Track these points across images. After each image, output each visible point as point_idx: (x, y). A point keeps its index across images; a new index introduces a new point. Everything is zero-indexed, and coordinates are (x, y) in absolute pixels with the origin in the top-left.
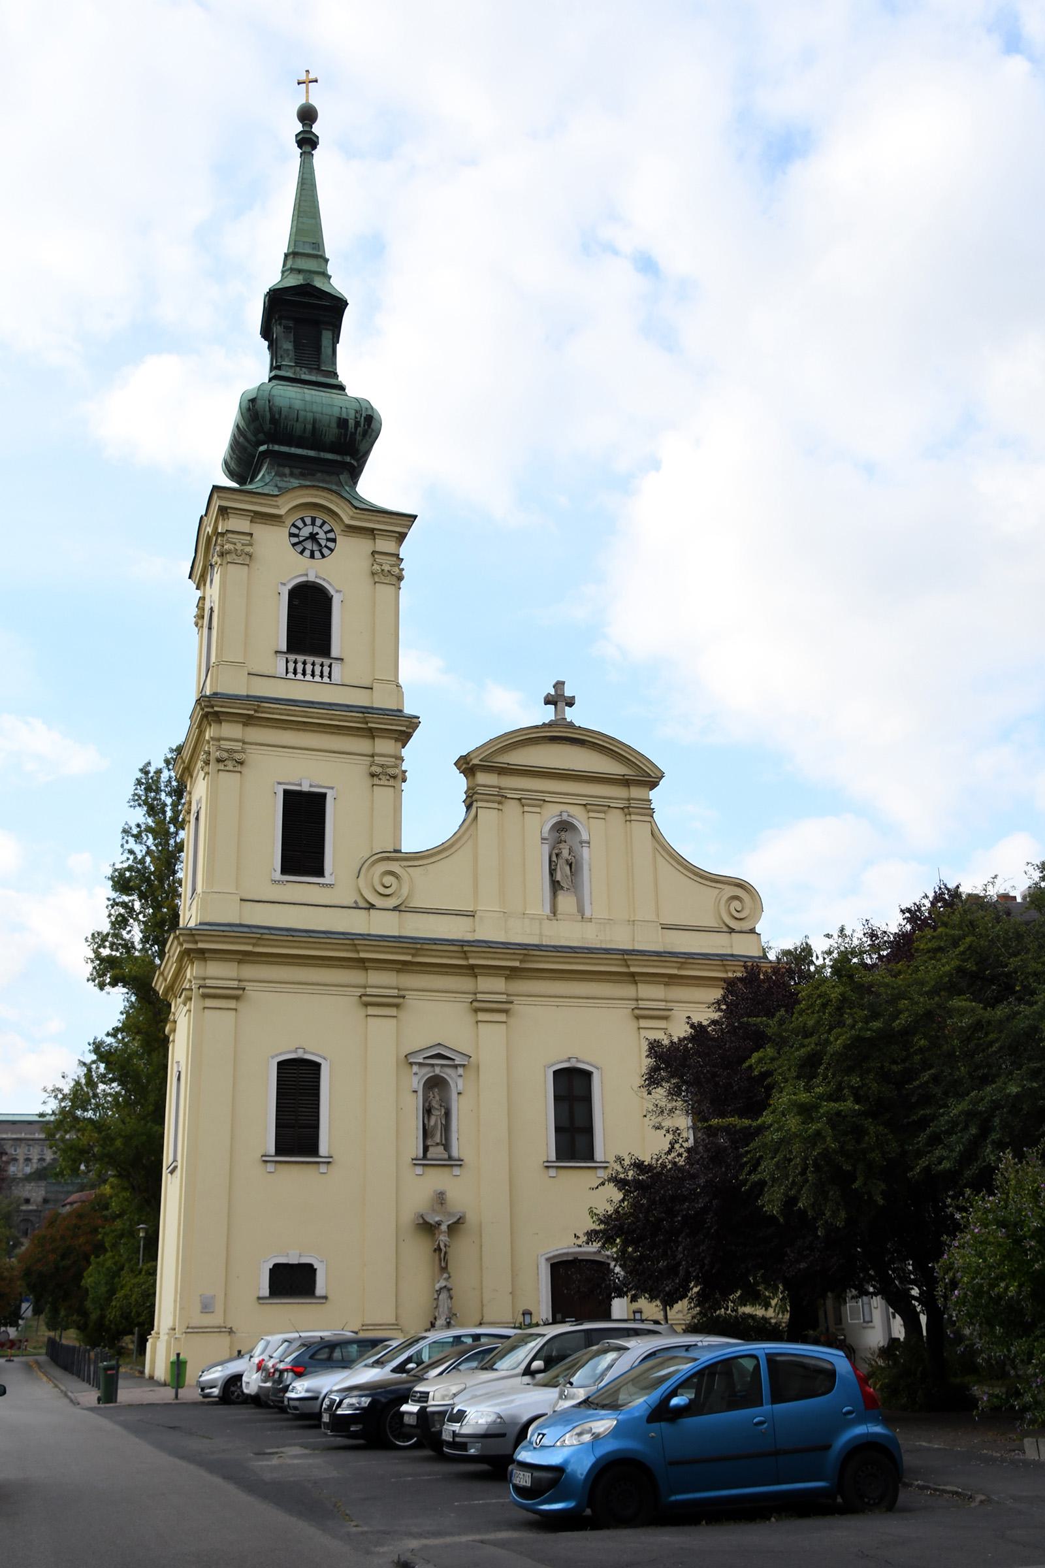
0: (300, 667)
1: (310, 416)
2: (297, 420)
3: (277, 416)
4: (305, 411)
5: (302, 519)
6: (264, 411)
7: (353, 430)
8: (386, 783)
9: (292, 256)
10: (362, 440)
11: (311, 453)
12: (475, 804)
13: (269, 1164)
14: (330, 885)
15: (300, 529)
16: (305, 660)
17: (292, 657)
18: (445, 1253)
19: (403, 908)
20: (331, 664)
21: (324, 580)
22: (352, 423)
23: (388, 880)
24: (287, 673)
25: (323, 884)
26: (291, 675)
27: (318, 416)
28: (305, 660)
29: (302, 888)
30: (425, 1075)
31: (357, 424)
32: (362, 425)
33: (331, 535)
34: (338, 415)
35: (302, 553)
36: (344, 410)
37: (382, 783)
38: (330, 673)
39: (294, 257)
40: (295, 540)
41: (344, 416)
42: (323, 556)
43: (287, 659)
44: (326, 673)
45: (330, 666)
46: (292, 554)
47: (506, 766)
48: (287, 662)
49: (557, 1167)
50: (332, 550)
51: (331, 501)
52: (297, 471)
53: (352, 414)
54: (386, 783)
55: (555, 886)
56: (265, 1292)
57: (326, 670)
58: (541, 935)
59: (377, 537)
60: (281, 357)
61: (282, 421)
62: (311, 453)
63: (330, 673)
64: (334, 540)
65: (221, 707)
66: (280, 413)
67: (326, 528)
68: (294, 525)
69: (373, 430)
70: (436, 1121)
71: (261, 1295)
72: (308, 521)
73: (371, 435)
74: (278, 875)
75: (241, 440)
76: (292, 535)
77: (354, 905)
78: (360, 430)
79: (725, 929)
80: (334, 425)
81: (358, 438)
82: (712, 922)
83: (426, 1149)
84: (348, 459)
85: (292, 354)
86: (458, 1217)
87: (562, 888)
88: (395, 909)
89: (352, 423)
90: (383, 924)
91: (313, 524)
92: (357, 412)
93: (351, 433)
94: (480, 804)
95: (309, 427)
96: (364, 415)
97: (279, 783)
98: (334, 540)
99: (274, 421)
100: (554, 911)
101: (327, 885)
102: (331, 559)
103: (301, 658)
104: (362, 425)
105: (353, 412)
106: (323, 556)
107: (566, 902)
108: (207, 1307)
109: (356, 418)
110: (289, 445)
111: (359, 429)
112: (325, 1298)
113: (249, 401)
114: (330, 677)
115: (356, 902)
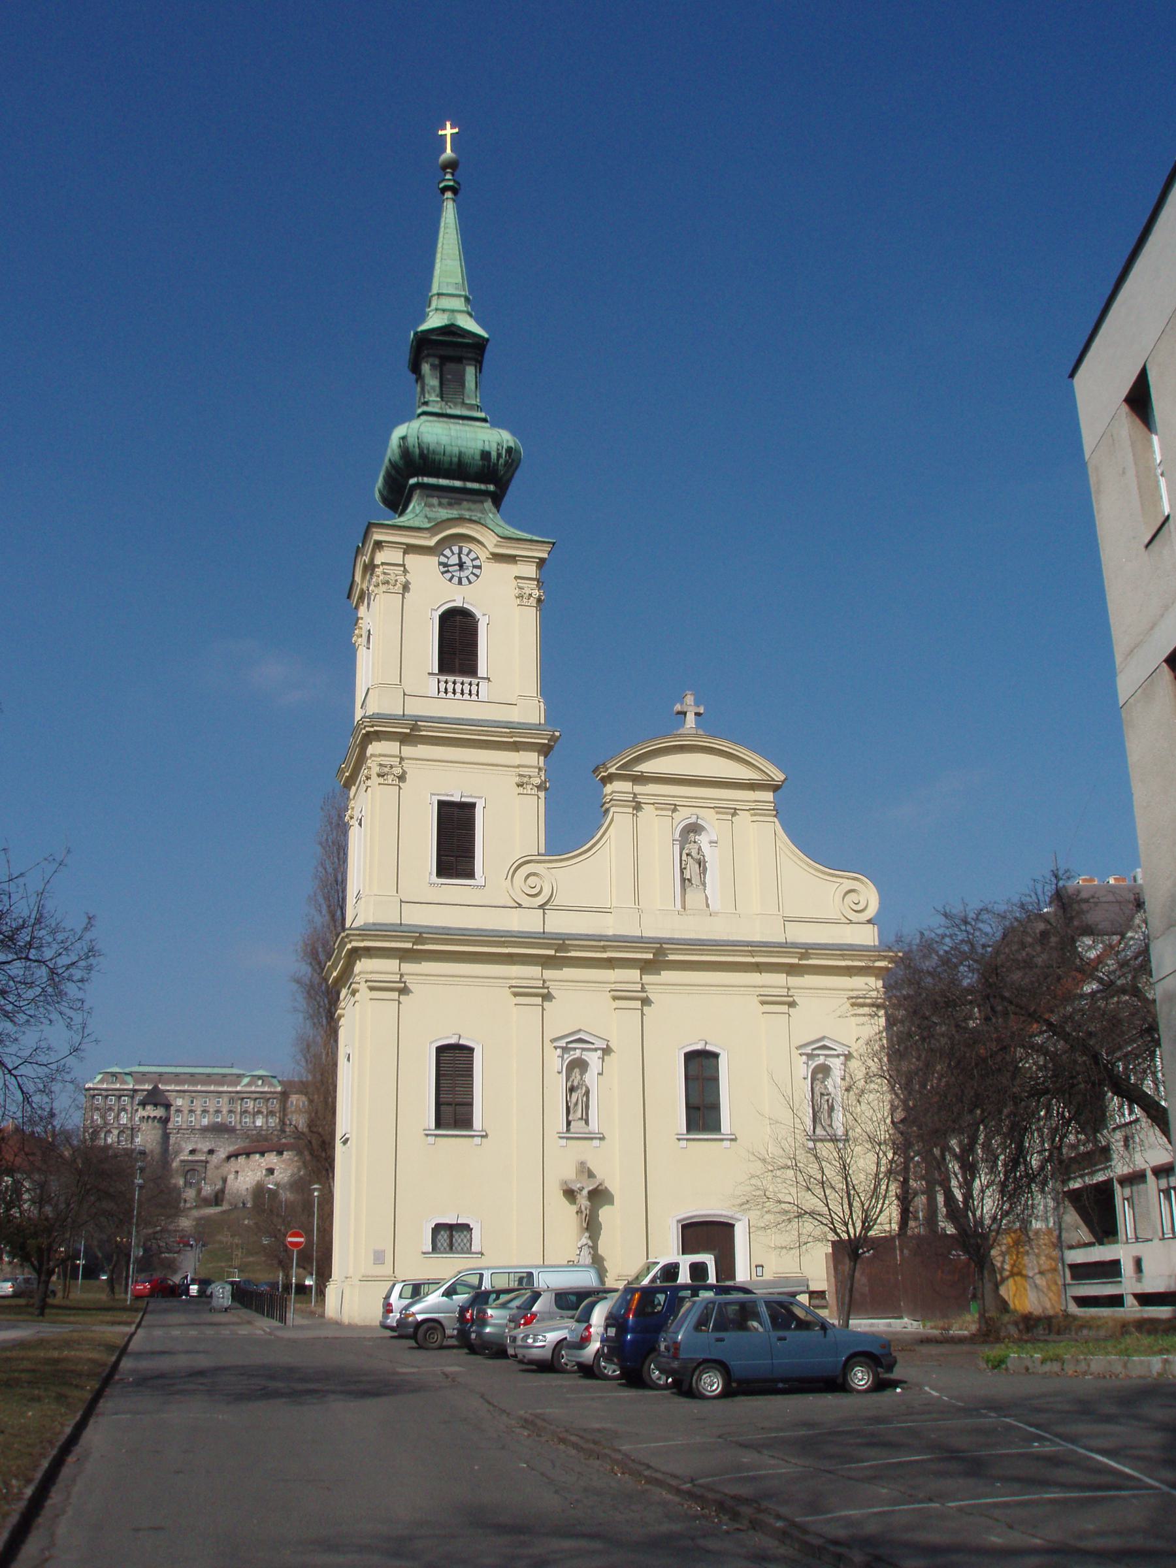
0: (450, 687)
2: (444, 455)
3: (425, 452)
4: (451, 445)
6: (414, 447)
9: (436, 297)
11: (458, 484)
12: (613, 809)
13: (429, 1138)
15: (448, 558)
17: (443, 678)
20: (479, 682)
21: (471, 604)
22: (494, 454)
23: (532, 881)
25: (474, 886)
26: (442, 694)
27: (463, 450)
29: (455, 888)
31: (499, 456)
32: (504, 456)
33: (477, 563)
34: (482, 448)
36: (487, 443)
38: (478, 692)
39: (438, 298)
41: (487, 448)
42: (470, 582)
44: (474, 691)
45: (478, 685)
46: (442, 580)
48: (439, 682)
50: (478, 576)
51: (477, 531)
52: (445, 501)
53: (494, 446)
60: (429, 392)
61: (430, 456)
62: (458, 484)
63: (478, 692)
64: (479, 567)
66: (428, 449)
67: (472, 556)
71: (424, 1251)
75: (393, 472)
80: (478, 457)
82: (834, 915)
83: (569, 1123)
86: (598, 1184)
89: (494, 454)
93: (494, 464)
96: (505, 446)
97: (432, 794)
98: (479, 567)
99: (423, 455)
102: (478, 584)
103: (451, 679)
104: (504, 456)
106: (470, 582)
107: (694, 897)
108: (379, 1258)
109: (498, 450)
113: (400, 438)
114: (477, 695)
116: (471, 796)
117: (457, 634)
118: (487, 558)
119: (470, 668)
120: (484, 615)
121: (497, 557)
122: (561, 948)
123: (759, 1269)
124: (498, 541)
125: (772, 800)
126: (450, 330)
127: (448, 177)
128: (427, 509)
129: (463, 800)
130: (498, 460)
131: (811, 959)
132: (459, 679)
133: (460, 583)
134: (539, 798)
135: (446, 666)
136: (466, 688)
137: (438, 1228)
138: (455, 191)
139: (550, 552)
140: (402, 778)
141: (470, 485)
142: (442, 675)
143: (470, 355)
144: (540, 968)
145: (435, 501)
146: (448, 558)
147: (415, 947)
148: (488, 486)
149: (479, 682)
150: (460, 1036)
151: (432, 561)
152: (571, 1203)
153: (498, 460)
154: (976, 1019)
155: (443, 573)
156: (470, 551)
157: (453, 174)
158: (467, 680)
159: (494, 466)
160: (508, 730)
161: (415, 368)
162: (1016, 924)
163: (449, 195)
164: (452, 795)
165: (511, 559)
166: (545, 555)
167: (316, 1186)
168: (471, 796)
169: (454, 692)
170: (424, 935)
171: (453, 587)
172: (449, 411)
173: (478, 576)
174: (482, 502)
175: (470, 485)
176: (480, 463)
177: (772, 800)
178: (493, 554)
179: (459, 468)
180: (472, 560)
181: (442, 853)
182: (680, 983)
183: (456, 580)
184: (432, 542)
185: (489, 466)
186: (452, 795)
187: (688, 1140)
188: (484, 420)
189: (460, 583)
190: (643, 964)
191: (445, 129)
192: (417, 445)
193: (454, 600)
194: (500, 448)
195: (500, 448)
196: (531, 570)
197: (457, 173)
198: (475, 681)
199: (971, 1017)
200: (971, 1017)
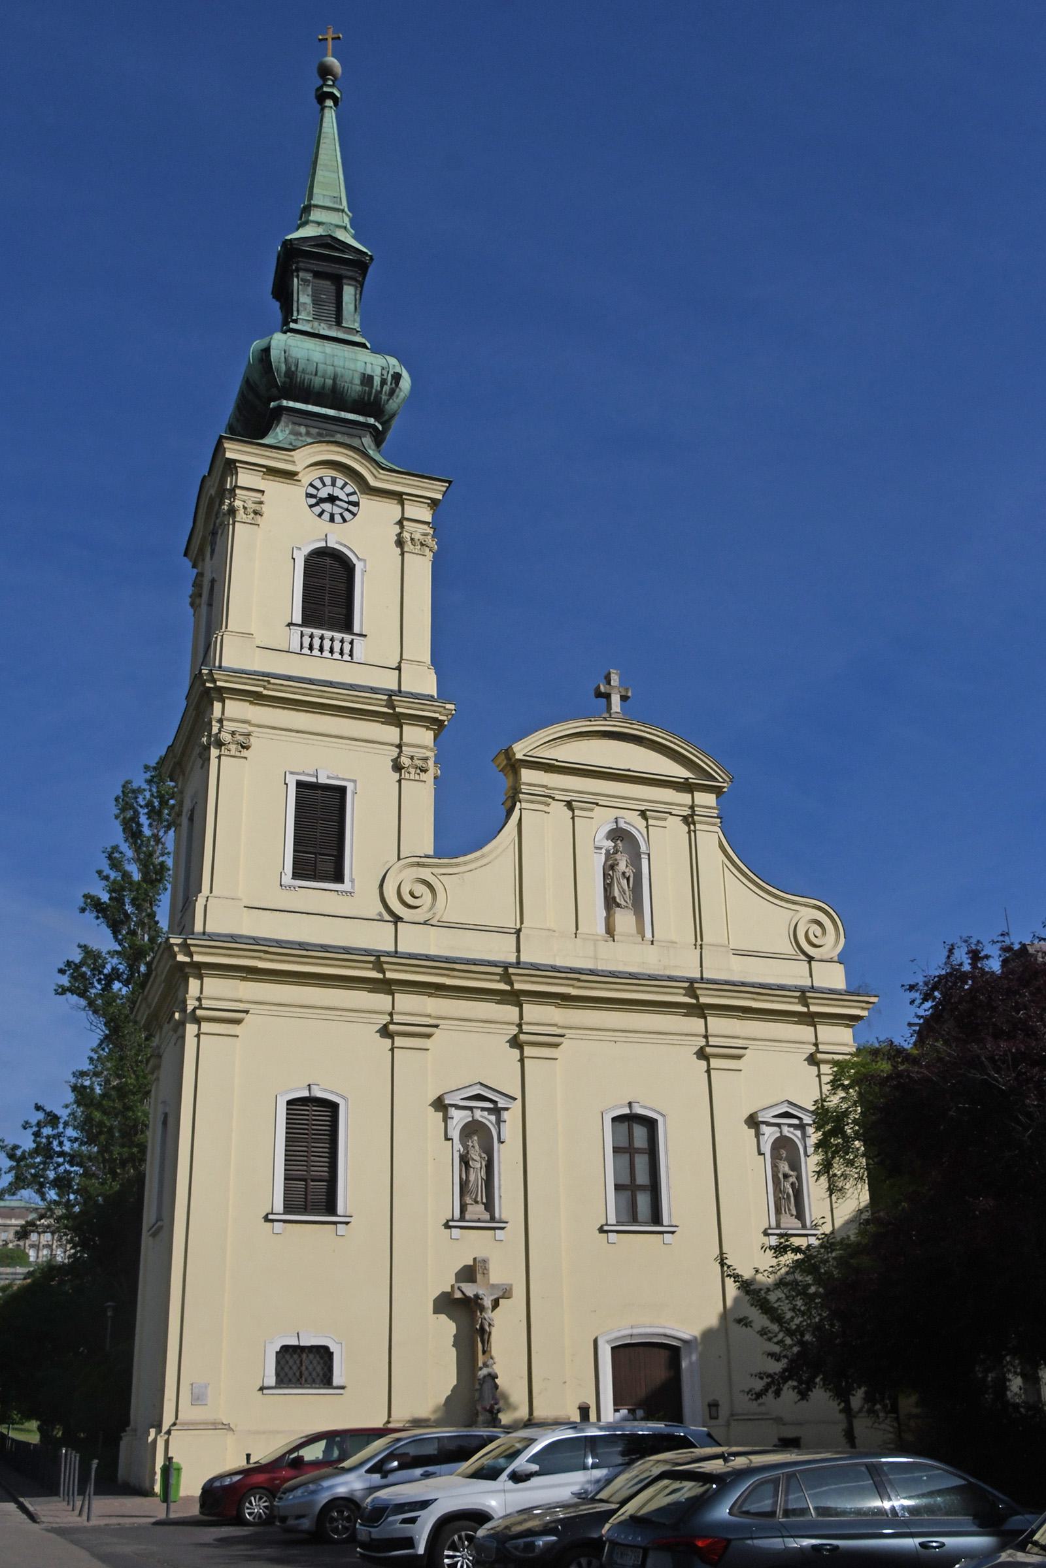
1: (330, 370)
2: (316, 375)
3: (293, 369)
5: (321, 479)
7: (379, 389)
8: (417, 777)
10: (388, 400)
11: (331, 412)
14: (351, 893)
15: (318, 490)
16: (323, 635)
17: (308, 631)
18: (490, 1333)
19: (434, 922)
20: (353, 640)
22: (377, 381)
23: (420, 889)
24: (302, 648)
25: (342, 892)
26: (306, 651)
27: (339, 370)
28: (323, 635)
30: (461, 1119)
31: (383, 382)
32: (389, 383)
34: (362, 371)
35: (320, 515)
36: (369, 366)
37: (412, 777)
38: (351, 650)
40: (313, 501)
41: (369, 372)
43: (302, 632)
45: (352, 643)
46: (309, 516)
49: (285, 1221)
50: (354, 515)
52: (314, 431)
54: (417, 777)
55: (610, 903)
56: (271, 1380)
57: (347, 647)
58: (596, 958)
59: (406, 502)
61: (299, 374)
62: (331, 412)
63: (351, 650)
64: (356, 504)
65: (226, 681)
66: (297, 366)
68: (311, 485)
69: (400, 389)
70: (476, 1176)
72: (328, 481)
73: (398, 396)
74: (288, 878)
76: (309, 495)
77: (378, 918)
78: (386, 388)
80: (357, 381)
81: (384, 397)
84: (372, 421)
85: (310, 308)
87: (619, 905)
88: (425, 923)
89: (377, 381)
90: (414, 940)
91: (333, 484)
92: (383, 368)
94: (524, 805)
95: (329, 382)
96: (391, 372)
98: (356, 504)
99: (290, 374)
100: (610, 931)
101: (346, 892)
102: (353, 524)
103: (318, 632)
104: (389, 383)
105: (380, 368)
106: (345, 521)
109: (382, 375)
110: (307, 402)
111: (385, 387)
112: (343, 1388)
114: (351, 655)
115: (380, 914)
117: (327, 592)
119: (345, 623)
123: (714, 1409)
125: (715, 805)
126: (329, 242)
128: (292, 437)
130: (382, 387)
132: (328, 634)
133: (332, 519)
137: (286, 1352)
139: (445, 492)
141: (344, 415)
142: (307, 627)
143: (350, 274)
145: (303, 430)
146: (318, 490)
148: (368, 418)
149: (353, 640)
152: (457, 1274)
153: (382, 387)
155: (311, 506)
158: (338, 636)
159: (376, 396)
161: (283, 294)
163: (329, 103)
166: (440, 497)
167: (109, 1304)
169: (321, 650)
171: (324, 525)
172: (322, 332)
173: (354, 515)
175: (344, 415)
176: (359, 388)
177: (715, 805)
179: (333, 395)
181: (301, 848)
182: (598, 1026)
183: (326, 516)
185: (370, 394)
187: (285, 1221)
188: (363, 346)
189: (332, 519)
191: (327, 33)
192: (283, 359)
194: (385, 373)
195: (385, 373)
198: (348, 637)
199: (169, 815)
200: (169, 815)
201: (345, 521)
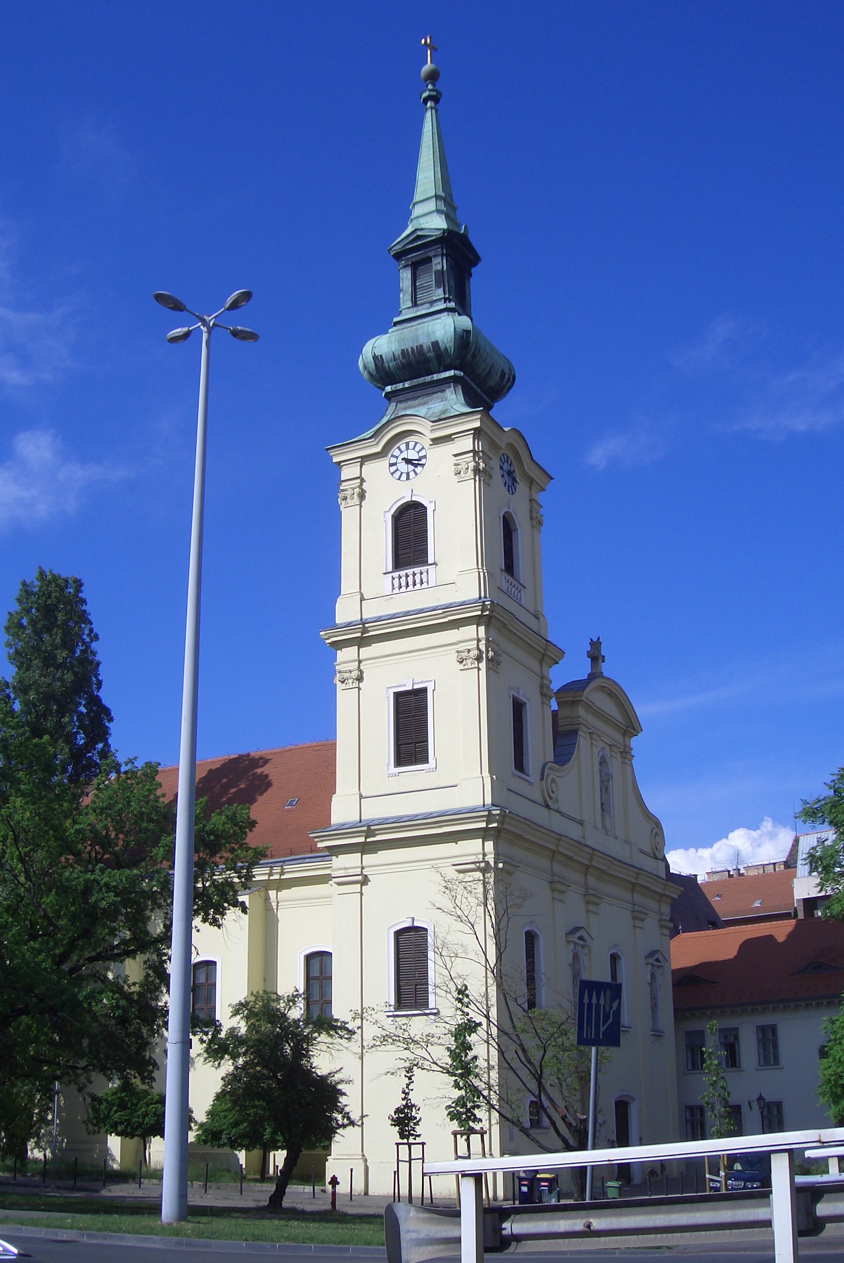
2: (485, 361)
16: (406, 573)
29: (413, 775)
42: (392, 474)
47: (592, 704)
79: (653, 856)
103: (410, 571)
113: (464, 330)
116: (422, 682)
118: (431, 445)
120: (431, 502)
121: (436, 441)
122: (369, 833)
124: (432, 426)
127: (430, 87)
129: (416, 687)
131: (377, 835)
134: (479, 669)
135: (399, 562)
136: (418, 578)
138: (436, 99)
140: (360, 679)
144: (360, 854)
147: (368, 840)
150: (413, 919)
151: (382, 464)
154: (13, 964)
156: (416, 443)
157: (434, 85)
160: (440, 611)
162: (248, 783)
164: (405, 685)
165: (448, 439)
166: (477, 424)
168: (422, 682)
170: (372, 828)
174: (443, 391)
178: (432, 440)
180: (401, 452)
184: (378, 449)
186: (405, 685)
190: (482, 833)
193: (404, 497)
196: (467, 443)
197: (438, 83)
201: (392, 474)
